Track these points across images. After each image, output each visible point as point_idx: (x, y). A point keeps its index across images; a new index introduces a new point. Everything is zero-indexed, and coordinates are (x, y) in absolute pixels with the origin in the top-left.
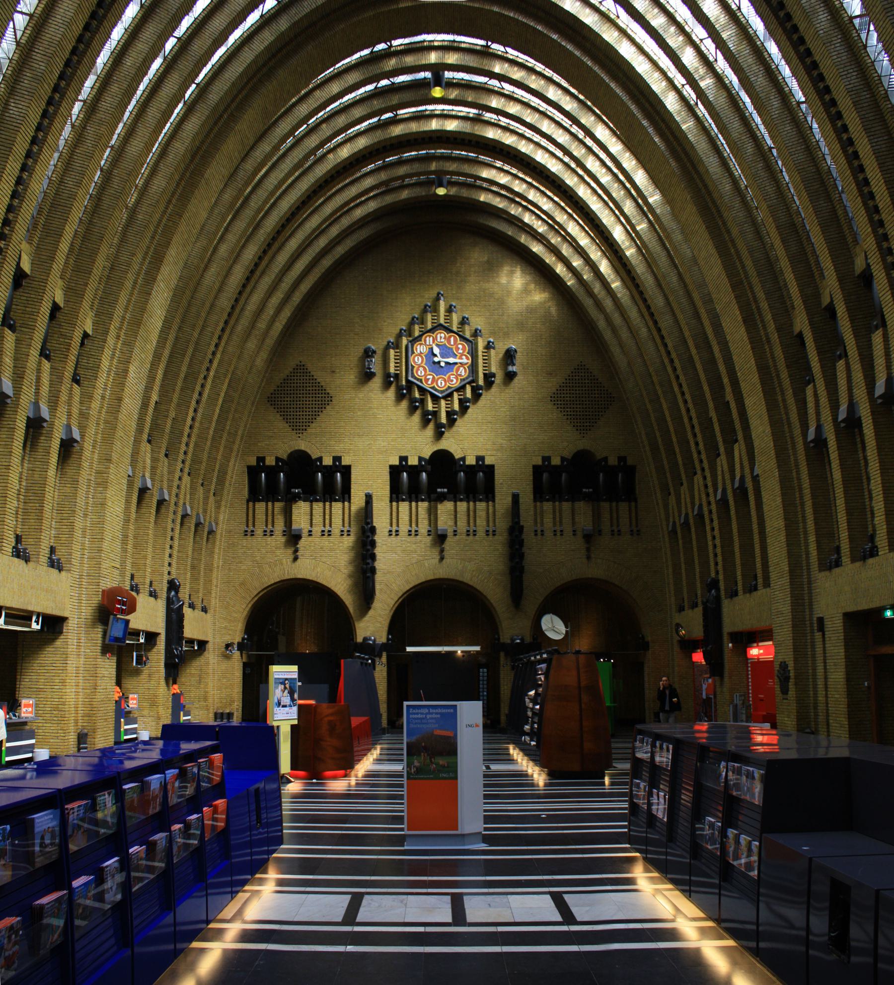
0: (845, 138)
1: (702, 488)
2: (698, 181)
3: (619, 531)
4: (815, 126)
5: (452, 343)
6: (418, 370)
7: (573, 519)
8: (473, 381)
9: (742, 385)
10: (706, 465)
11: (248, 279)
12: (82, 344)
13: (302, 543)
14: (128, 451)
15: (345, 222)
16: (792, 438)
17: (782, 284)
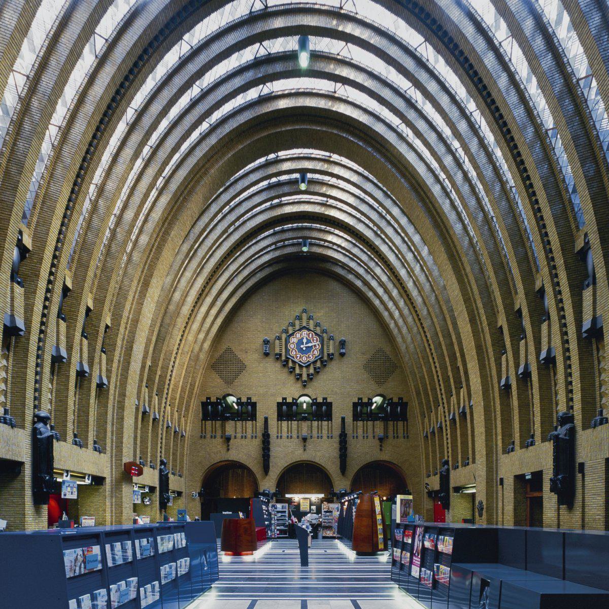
0: (536, 208)
1: (442, 414)
2: (449, 239)
3: (397, 436)
4: (519, 201)
5: (311, 336)
6: (292, 351)
7: (373, 430)
8: (322, 358)
9: (467, 356)
10: (445, 401)
11: (198, 299)
12: (106, 332)
13: (232, 441)
14: (135, 391)
15: (253, 266)
16: (492, 384)
17: (493, 299)
